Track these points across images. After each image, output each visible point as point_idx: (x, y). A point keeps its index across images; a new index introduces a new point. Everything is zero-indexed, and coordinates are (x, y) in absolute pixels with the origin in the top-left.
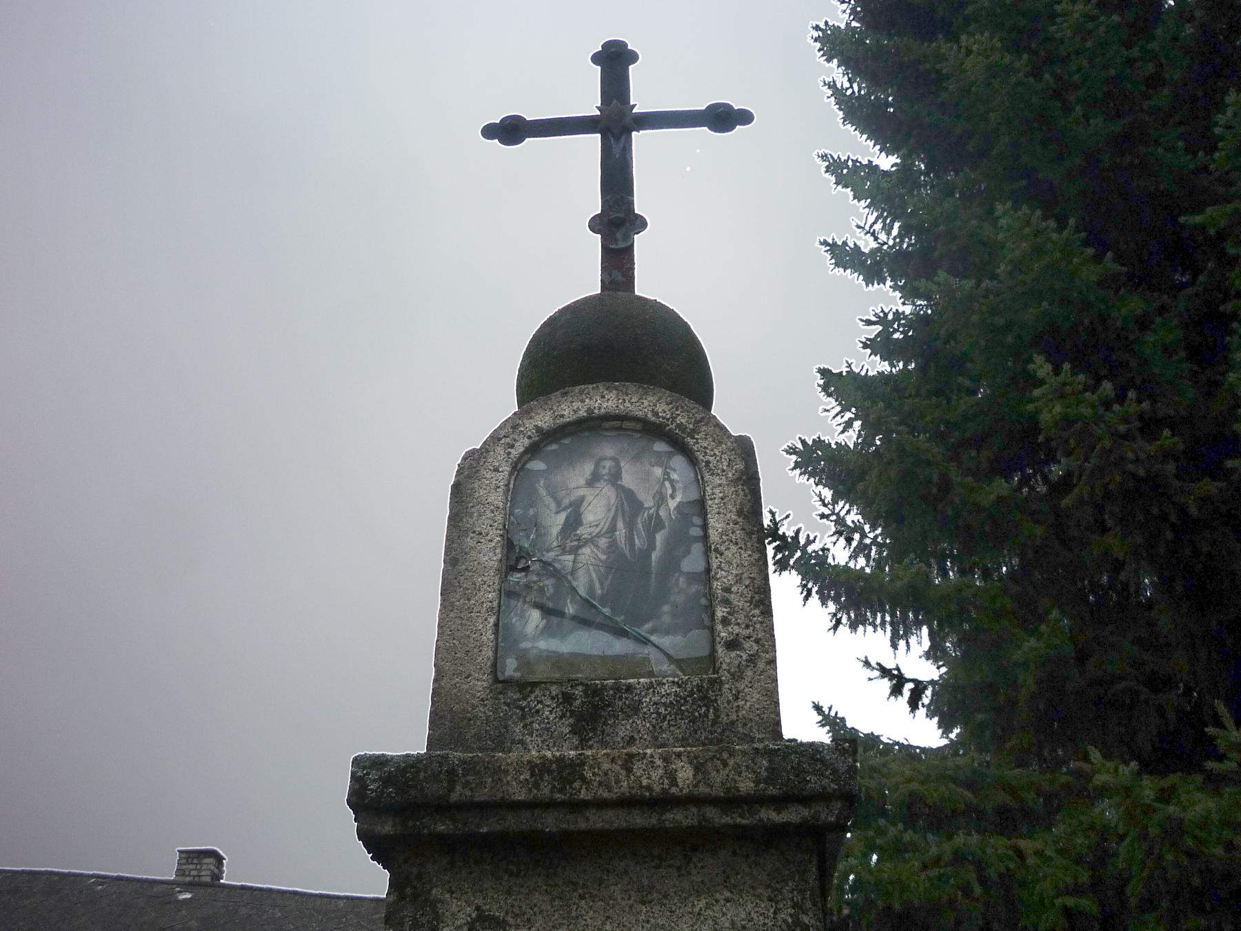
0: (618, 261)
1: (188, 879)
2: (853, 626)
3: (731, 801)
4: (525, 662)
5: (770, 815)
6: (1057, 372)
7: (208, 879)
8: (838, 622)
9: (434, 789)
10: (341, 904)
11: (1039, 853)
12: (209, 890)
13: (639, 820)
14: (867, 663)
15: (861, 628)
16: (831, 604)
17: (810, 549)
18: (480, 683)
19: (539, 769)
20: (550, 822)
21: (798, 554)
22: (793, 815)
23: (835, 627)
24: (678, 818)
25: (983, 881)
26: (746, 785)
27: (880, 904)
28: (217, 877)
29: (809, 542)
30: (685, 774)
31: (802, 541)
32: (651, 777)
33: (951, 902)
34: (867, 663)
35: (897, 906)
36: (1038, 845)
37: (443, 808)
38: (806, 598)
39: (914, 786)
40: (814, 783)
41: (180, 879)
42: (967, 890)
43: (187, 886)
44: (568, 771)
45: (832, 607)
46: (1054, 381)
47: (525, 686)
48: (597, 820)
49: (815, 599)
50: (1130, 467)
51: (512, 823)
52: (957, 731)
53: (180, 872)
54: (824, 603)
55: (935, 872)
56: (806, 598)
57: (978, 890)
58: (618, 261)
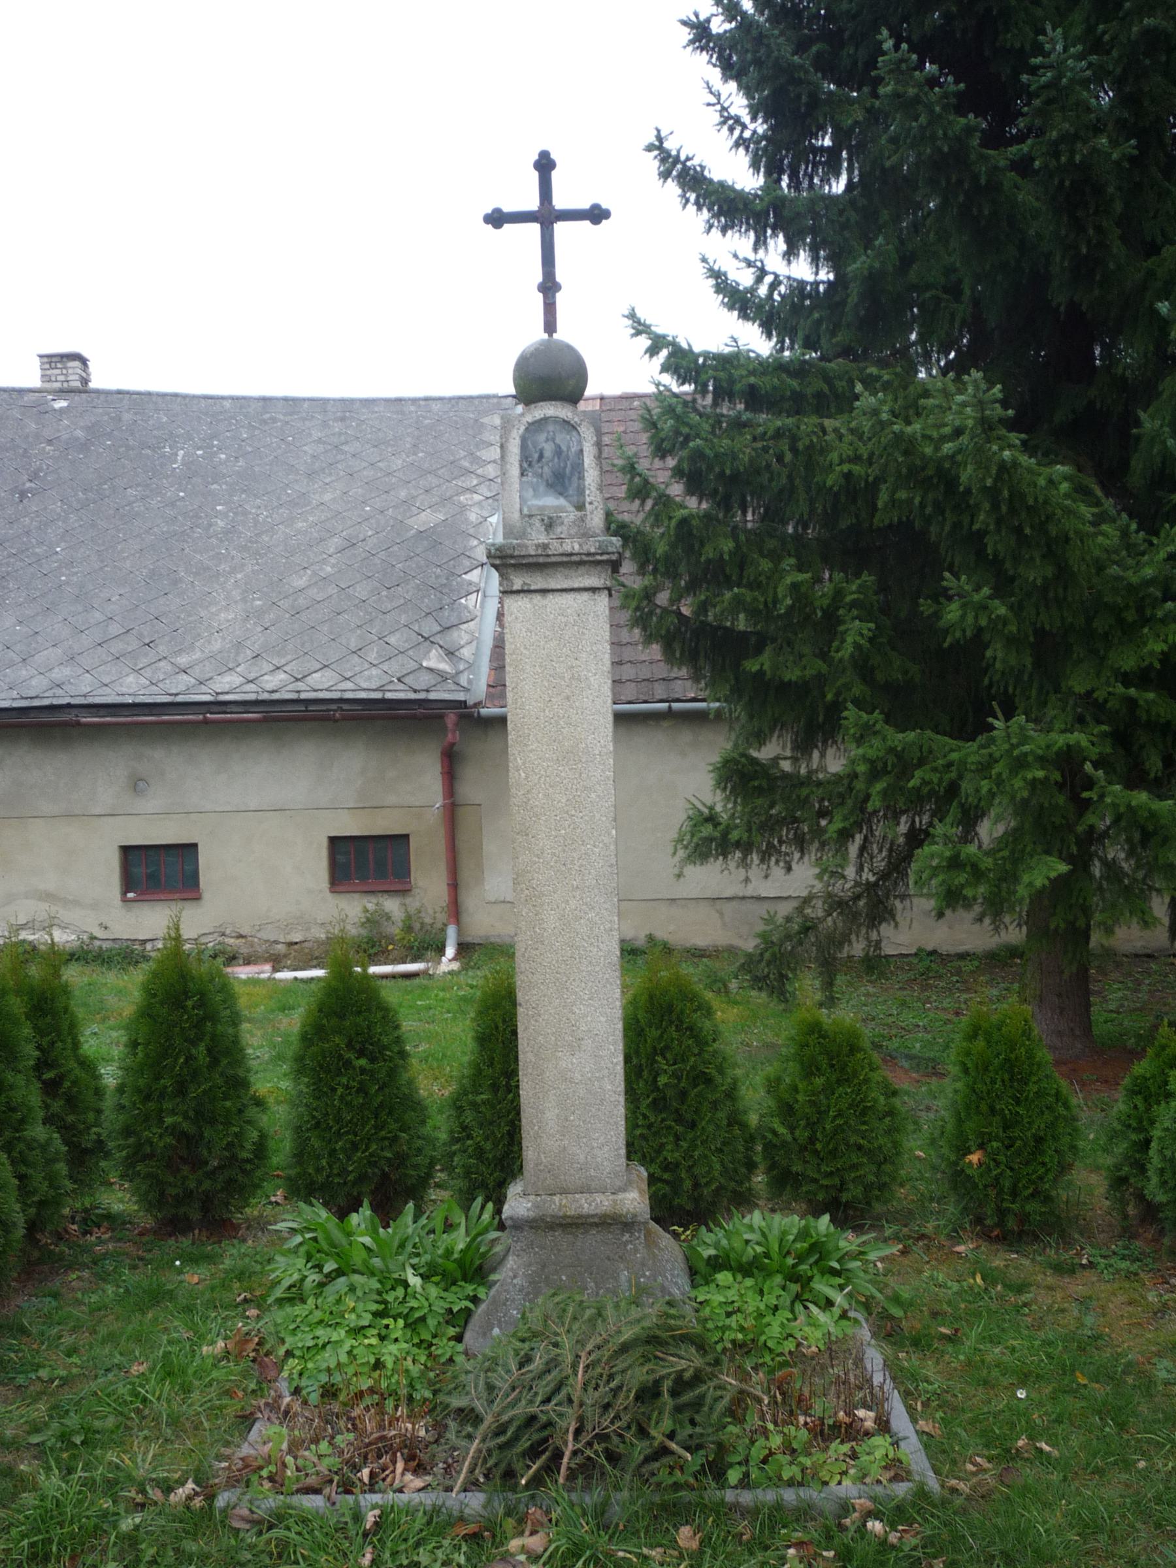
0: (550, 326)
1: (57, 385)
2: (724, 230)
3: (589, 554)
4: (529, 509)
5: (599, 558)
6: (897, 47)
7: (78, 384)
8: (711, 226)
9: (509, 552)
10: (227, 404)
11: (836, 430)
12: (84, 396)
13: (565, 559)
14: (735, 256)
15: (730, 233)
16: (705, 210)
17: (689, 164)
18: (517, 515)
19: (538, 546)
20: (541, 560)
21: (679, 166)
22: (605, 557)
23: (708, 231)
24: (574, 558)
25: (794, 449)
26: (593, 550)
27: (717, 469)
28: (85, 381)
29: (688, 159)
30: (577, 547)
31: (683, 158)
32: (567, 548)
33: (768, 466)
34: (735, 256)
35: (728, 472)
36: (837, 424)
37: (512, 557)
38: (684, 207)
39: (752, 380)
40: (610, 549)
41: (48, 385)
42: (780, 458)
43: (62, 392)
44: (545, 546)
45: (705, 214)
46: (893, 56)
47: (530, 516)
48: (553, 559)
49: (691, 208)
50: (939, 143)
51: (531, 560)
52: (962, 85)
53: (45, 378)
54: (699, 208)
55: (759, 445)
56: (684, 207)
57: (788, 457)
58: (550, 326)
